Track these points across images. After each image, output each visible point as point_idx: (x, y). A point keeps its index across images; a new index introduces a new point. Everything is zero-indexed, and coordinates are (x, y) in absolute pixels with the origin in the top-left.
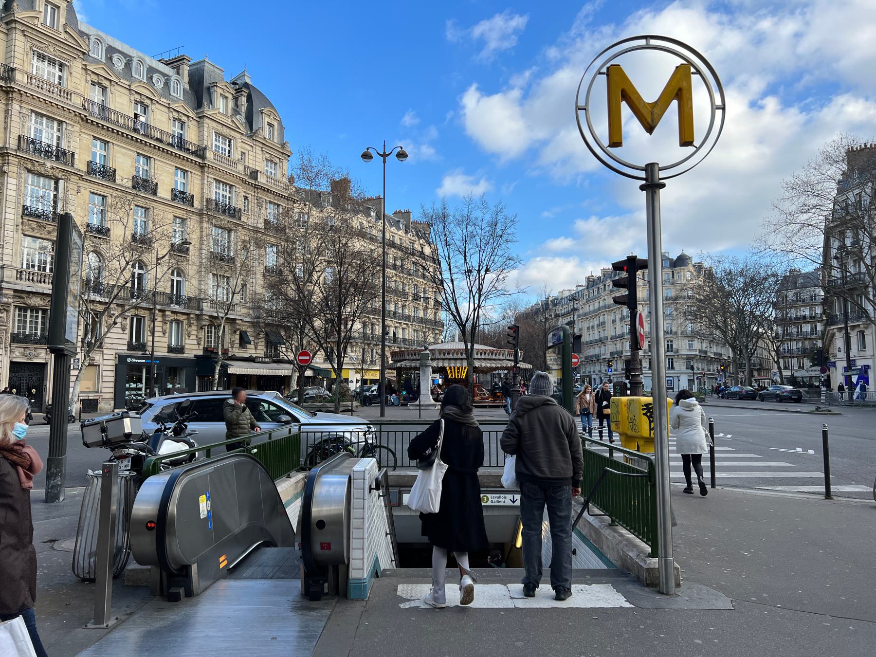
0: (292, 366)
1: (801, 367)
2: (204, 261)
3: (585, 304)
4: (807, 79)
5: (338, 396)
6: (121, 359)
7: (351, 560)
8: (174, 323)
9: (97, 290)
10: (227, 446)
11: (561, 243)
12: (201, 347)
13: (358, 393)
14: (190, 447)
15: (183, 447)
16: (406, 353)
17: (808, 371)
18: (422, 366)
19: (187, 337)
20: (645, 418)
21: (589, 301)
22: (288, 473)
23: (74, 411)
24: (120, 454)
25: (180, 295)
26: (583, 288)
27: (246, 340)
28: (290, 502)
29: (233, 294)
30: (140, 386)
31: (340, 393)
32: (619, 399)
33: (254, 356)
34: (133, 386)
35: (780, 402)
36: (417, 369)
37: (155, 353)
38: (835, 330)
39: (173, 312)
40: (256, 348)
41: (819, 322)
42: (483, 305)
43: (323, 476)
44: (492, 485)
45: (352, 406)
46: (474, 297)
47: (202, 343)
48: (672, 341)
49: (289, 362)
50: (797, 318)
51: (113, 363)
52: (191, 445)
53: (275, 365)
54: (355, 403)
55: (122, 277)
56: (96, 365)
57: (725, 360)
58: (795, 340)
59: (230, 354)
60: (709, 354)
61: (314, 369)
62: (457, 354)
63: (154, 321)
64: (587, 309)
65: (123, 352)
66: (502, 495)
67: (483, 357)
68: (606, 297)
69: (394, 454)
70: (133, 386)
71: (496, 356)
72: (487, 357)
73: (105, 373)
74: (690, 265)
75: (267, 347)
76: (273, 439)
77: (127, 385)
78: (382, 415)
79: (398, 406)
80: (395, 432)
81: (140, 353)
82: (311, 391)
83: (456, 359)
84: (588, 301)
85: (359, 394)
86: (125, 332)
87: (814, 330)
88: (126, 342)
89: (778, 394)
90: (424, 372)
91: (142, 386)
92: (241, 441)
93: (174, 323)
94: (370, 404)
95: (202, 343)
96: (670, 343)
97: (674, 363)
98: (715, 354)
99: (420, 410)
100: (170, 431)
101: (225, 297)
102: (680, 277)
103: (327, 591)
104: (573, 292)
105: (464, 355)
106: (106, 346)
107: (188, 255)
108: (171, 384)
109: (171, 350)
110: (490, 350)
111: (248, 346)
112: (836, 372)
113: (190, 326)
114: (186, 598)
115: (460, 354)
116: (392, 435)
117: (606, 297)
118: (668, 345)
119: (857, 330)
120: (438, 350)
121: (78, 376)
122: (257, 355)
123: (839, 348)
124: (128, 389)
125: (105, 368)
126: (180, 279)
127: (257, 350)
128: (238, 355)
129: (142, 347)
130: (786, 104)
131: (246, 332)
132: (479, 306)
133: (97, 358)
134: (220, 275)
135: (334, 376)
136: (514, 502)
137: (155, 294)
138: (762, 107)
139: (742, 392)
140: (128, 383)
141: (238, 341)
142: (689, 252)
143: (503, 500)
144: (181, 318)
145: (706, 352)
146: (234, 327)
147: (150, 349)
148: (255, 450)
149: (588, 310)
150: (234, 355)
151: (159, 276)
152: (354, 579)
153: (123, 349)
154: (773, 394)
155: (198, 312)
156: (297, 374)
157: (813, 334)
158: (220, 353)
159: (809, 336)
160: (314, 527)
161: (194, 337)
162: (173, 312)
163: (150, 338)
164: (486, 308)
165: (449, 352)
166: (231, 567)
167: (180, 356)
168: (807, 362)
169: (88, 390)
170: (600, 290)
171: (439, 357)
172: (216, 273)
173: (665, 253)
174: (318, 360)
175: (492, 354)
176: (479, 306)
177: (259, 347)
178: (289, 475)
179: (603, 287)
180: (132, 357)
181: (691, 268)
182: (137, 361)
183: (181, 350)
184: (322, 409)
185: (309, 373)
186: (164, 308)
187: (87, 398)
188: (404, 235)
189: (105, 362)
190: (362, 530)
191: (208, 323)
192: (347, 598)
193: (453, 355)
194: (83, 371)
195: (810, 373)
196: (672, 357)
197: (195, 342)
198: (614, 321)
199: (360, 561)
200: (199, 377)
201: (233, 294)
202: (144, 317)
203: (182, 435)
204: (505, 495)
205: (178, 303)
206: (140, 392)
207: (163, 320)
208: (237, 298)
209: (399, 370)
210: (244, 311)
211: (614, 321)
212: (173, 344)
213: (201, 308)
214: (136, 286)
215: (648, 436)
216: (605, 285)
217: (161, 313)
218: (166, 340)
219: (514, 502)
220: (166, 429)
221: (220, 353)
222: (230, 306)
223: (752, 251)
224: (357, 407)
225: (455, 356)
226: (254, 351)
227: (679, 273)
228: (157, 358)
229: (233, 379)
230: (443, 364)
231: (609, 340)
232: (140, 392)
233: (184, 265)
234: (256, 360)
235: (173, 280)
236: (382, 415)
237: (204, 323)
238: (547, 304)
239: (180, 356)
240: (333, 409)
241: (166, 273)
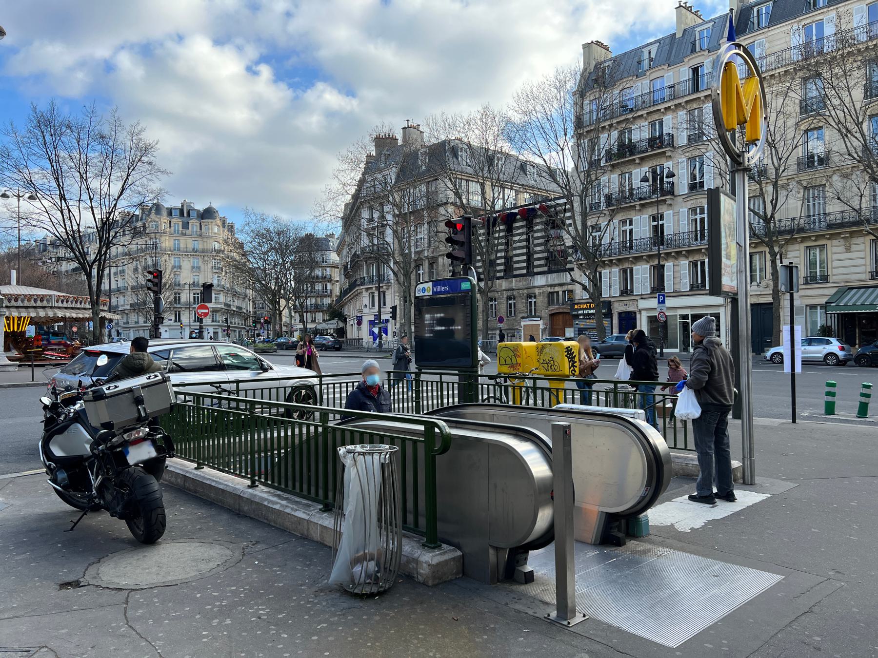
1: (313, 321)
4: (293, 60)
32: (517, 344)
35: (325, 351)
38: (364, 290)
41: (328, 282)
48: (179, 294)
57: (245, 313)
67: (65, 305)
71: (81, 303)
72: (69, 305)
74: (218, 219)
89: (324, 344)
96: (177, 295)
97: (181, 316)
98: (237, 307)
118: (194, 297)
119: (370, 291)
123: (366, 305)
130: (279, 77)
138: (256, 73)
139: (289, 343)
142: (215, 205)
145: (229, 306)
154: (320, 344)
157: (323, 292)
173: (191, 203)
175: (76, 302)
196: (180, 310)
225: (26, 304)
227: (206, 225)
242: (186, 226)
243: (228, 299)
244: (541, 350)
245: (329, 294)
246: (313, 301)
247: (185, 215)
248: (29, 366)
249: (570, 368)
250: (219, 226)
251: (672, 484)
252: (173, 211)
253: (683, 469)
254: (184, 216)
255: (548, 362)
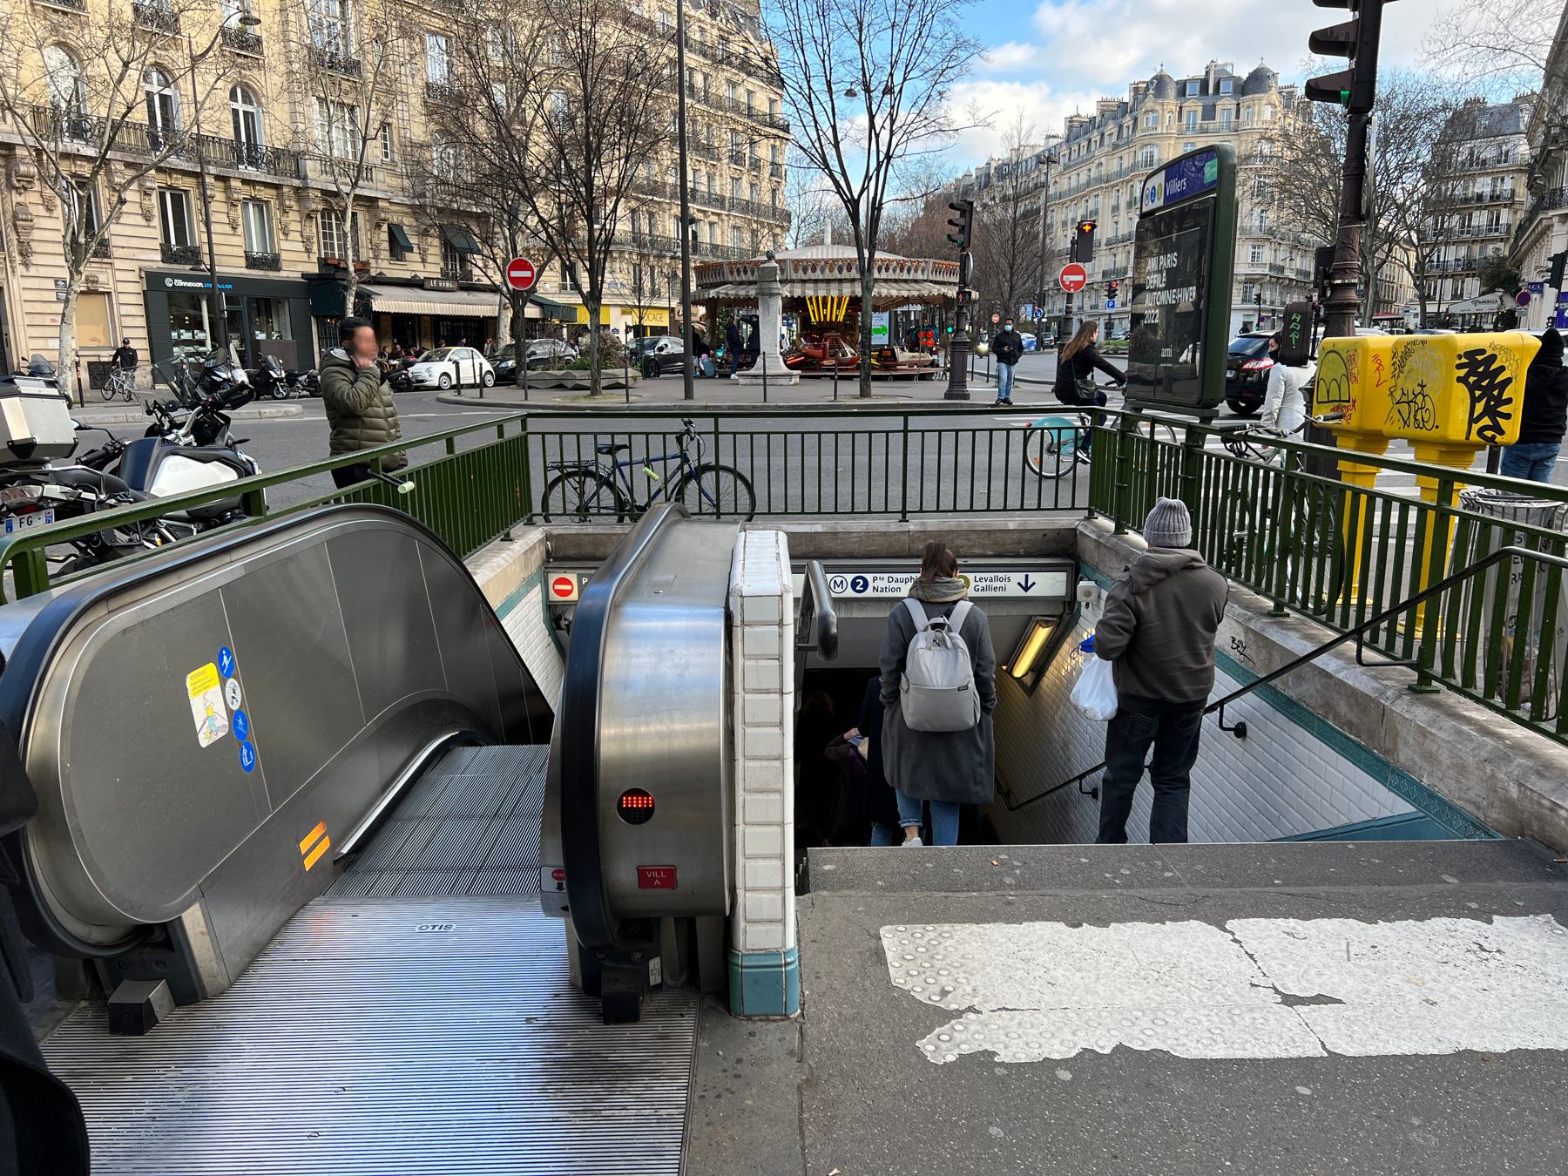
0: (497, 298)
2: (296, 67)
3: (1061, 174)
5: (597, 356)
6: (153, 280)
7: (740, 892)
8: (251, 205)
9: (78, 131)
10: (334, 473)
11: (1013, 55)
12: (314, 258)
13: (633, 352)
14: (240, 476)
15: (219, 475)
16: (726, 269)
17: (1475, 302)
18: (763, 295)
19: (282, 237)
20: (1461, 392)
21: (1070, 167)
22: (505, 531)
23: (70, 385)
24: (19, 499)
25: (256, 145)
26: (1060, 141)
27: (402, 242)
28: (510, 604)
29: (365, 140)
30: (200, 335)
31: (600, 351)
33: (422, 276)
34: (186, 335)
36: (752, 302)
37: (217, 269)
38: (1556, 220)
39: (245, 182)
40: (424, 261)
41: (1505, 206)
42: (898, 152)
43: (629, 609)
44: (977, 551)
45: (626, 377)
46: (877, 136)
47: (315, 248)
49: (494, 289)
50: (1467, 200)
51: (138, 288)
52: (244, 470)
53: (464, 295)
54: (631, 372)
55: (119, 99)
56: (103, 293)
58: (1454, 243)
59: (373, 273)
60: (1287, 273)
61: (540, 304)
62: (831, 270)
63: (206, 200)
64: (1064, 184)
65: (154, 265)
66: (1000, 575)
68: (1103, 160)
69: (750, 487)
70: (186, 335)
71: (909, 272)
72: (891, 275)
73: (124, 310)
75: (445, 258)
76: (458, 451)
77: (174, 335)
78: (689, 394)
79: (713, 377)
80: (820, 433)
81: (186, 268)
82: (540, 348)
83: (828, 281)
84: (1066, 167)
85: (636, 354)
86: (152, 224)
87: (1494, 223)
88: (156, 245)
90: (768, 307)
91: (205, 335)
92: (368, 459)
93: (251, 205)
94: (657, 375)
95: (315, 248)
98: (1299, 272)
99: (765, 385)
100: (182, 432)
101: (350, 149)
102: (1250, 116)
103: (659, 980)
104: (1038, 151)
105: (854, 271)
106: (117, 252)
107: (262, 54)
108: (262, 332)
109: (252, 262)
110: (898, 262)
111: (408, 255)
112: (1541, 303)
113: (285, 212)
114: (179, 1012)
115: (836, 271)
116: (743, 441)
117: (1103, 160)
120: (793, 261)
121: (64, 315)
122: (427, 275)
124: (180, 343)
125: (124, 298)
126: (249, 109)
127: (427, 261)
128: (389, 274)
129: (191, 256)
131: (399, 227)
132: (888, 157)
133: (102, 278)
134: (332, 102)
135: (583, 317)
136: (1026, 589)
137: (200, 140)
140: (174, 330)
141: (386, 245)
143: (1002, 584)
144: (264, 194)
145: (1282, 269)
146: (375, 216)
147: (206, 259)
148: (409, 486)
149: (1066, 187)
150: (381, 273)
151: (200, 98)
152: (753, 954)
153: (155, 260)
155: (297, 183)
156: (510, 314)
157: (1490, 230)
158: (352, 269)
159: (1482, 236)
160: (608, 808)
161: (297, 236)
162: (245, 182)
163: (205, 238)
164: (908, 158)
165: (814, 265)
166: (345, 851)
167: (272, 275)
168: (1473, 286)
169: (95, 344)
170: (1093, 144)
171: (794, 276)
172: (322, 95)
173: (1226, 64)
174: (547, 286)
176: (888, 157)
177: (430, 259)
178: (508, 535)
179: (1098, 138)
180: (174, 276)
181: (1274, 97)
182: (185, 284)
183: (273, 263)
184: (564, 383)
185: (531, 312)
186: (224, 172)
187: (95, 359)
188: (709, 20)
189: (121, 287)
190: (777, 796)
191: (320, 207)
192: (729, 1010)
193: (823, 271)
194: (73, 304)
195: (1480, 306)
197: (301, 247)
198: (1116, 209)
199: (772, 895)
200: (317, 318)
201: (365, 140)
202: (185, 191)
203: (220, 443)
204: (1008, 574)
205: (253, 162)
206: (202, 349)
207: (228, 198)
208: (374, 152)
209: (712, 304)
210: (396, 182)
211: (1116, 209)
212: (255, 250)
213: (302, 174)
214: (159, 124)
215: (1463, 438)
216: (1103, 135)
217: (221, 184)
218: (239, 241)
219: (1026, 589)
220: (175, 426)
221: (352, 269)
222: (361, 170)
223: (1427, 48)
224: (635, 378)
225: (828, 275)
226: (420, 267)
227: (1249, 107)
228: (225, 279)
229: (386, 324)
230: (803, 292)
231: (1103, 247)
232: (202, 349)
233: (255, 77)
234: (427, 286)
235: (235, 112)
236: (689, 394)
237: (314, 206)
238: (988, 175)
239: (272, 275)
240: (587, 383)
241: (213, 88)
242: (1209, 113)
243: (1281, 255)
244: (1402, 357)
245: (1504, 235)
246: (1463, 251)
247: (1211, 91)
248: (832, 377)
249: (1472, 420)
250: (1274, 106)
251: (389, 880)
252: (1188, 85)
253: (1540, 818)
254: (1207, 94)
255: (1411, 397)
